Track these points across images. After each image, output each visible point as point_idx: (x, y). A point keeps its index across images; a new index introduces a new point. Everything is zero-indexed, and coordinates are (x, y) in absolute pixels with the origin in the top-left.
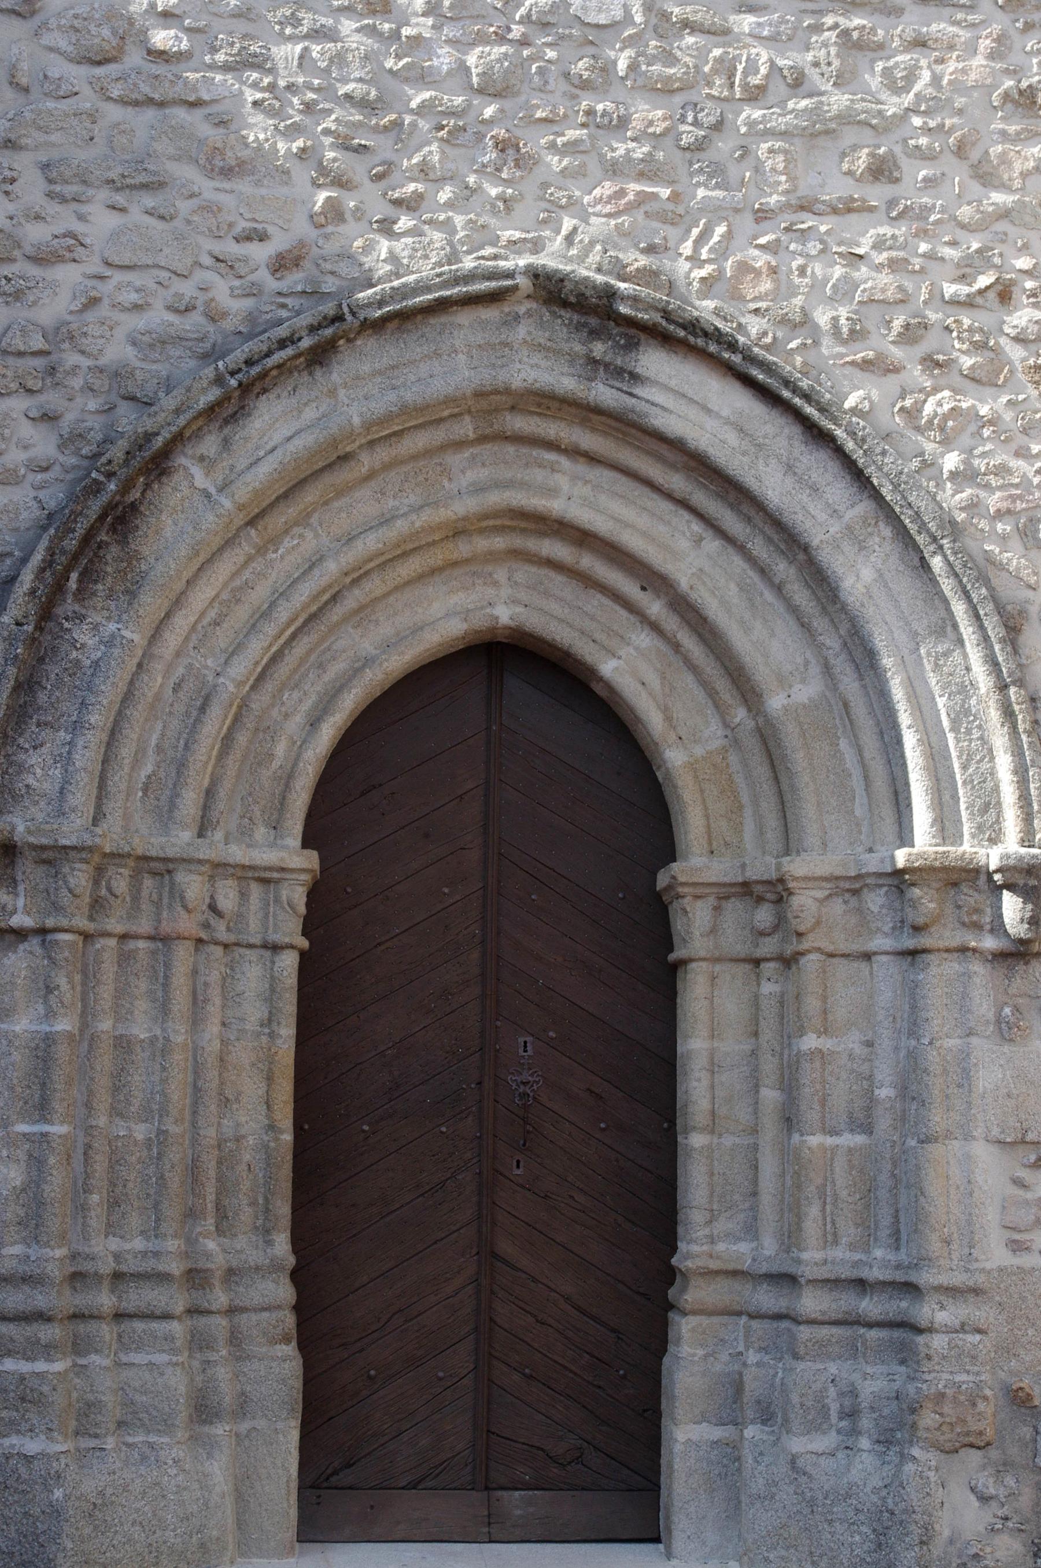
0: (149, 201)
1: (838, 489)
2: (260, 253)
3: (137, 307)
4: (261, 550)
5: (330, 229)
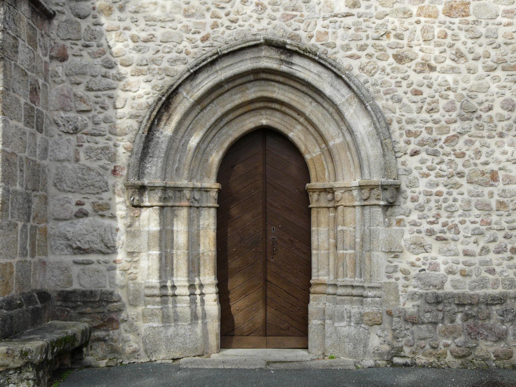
0: (170, 24)
1: (345, 90)
2: (198, 37)
3: (169, 52)
4: (202, 110)
5: (215, 29)
